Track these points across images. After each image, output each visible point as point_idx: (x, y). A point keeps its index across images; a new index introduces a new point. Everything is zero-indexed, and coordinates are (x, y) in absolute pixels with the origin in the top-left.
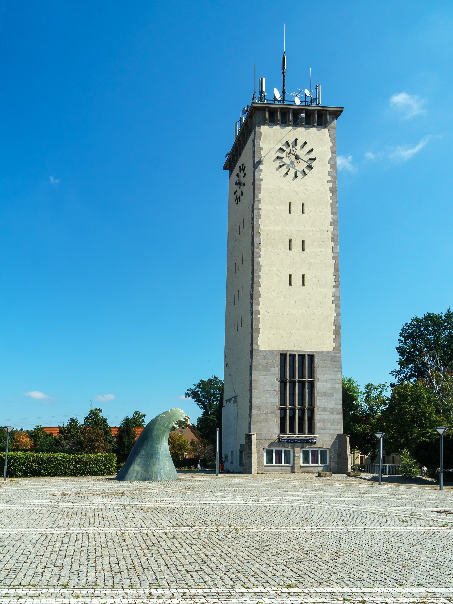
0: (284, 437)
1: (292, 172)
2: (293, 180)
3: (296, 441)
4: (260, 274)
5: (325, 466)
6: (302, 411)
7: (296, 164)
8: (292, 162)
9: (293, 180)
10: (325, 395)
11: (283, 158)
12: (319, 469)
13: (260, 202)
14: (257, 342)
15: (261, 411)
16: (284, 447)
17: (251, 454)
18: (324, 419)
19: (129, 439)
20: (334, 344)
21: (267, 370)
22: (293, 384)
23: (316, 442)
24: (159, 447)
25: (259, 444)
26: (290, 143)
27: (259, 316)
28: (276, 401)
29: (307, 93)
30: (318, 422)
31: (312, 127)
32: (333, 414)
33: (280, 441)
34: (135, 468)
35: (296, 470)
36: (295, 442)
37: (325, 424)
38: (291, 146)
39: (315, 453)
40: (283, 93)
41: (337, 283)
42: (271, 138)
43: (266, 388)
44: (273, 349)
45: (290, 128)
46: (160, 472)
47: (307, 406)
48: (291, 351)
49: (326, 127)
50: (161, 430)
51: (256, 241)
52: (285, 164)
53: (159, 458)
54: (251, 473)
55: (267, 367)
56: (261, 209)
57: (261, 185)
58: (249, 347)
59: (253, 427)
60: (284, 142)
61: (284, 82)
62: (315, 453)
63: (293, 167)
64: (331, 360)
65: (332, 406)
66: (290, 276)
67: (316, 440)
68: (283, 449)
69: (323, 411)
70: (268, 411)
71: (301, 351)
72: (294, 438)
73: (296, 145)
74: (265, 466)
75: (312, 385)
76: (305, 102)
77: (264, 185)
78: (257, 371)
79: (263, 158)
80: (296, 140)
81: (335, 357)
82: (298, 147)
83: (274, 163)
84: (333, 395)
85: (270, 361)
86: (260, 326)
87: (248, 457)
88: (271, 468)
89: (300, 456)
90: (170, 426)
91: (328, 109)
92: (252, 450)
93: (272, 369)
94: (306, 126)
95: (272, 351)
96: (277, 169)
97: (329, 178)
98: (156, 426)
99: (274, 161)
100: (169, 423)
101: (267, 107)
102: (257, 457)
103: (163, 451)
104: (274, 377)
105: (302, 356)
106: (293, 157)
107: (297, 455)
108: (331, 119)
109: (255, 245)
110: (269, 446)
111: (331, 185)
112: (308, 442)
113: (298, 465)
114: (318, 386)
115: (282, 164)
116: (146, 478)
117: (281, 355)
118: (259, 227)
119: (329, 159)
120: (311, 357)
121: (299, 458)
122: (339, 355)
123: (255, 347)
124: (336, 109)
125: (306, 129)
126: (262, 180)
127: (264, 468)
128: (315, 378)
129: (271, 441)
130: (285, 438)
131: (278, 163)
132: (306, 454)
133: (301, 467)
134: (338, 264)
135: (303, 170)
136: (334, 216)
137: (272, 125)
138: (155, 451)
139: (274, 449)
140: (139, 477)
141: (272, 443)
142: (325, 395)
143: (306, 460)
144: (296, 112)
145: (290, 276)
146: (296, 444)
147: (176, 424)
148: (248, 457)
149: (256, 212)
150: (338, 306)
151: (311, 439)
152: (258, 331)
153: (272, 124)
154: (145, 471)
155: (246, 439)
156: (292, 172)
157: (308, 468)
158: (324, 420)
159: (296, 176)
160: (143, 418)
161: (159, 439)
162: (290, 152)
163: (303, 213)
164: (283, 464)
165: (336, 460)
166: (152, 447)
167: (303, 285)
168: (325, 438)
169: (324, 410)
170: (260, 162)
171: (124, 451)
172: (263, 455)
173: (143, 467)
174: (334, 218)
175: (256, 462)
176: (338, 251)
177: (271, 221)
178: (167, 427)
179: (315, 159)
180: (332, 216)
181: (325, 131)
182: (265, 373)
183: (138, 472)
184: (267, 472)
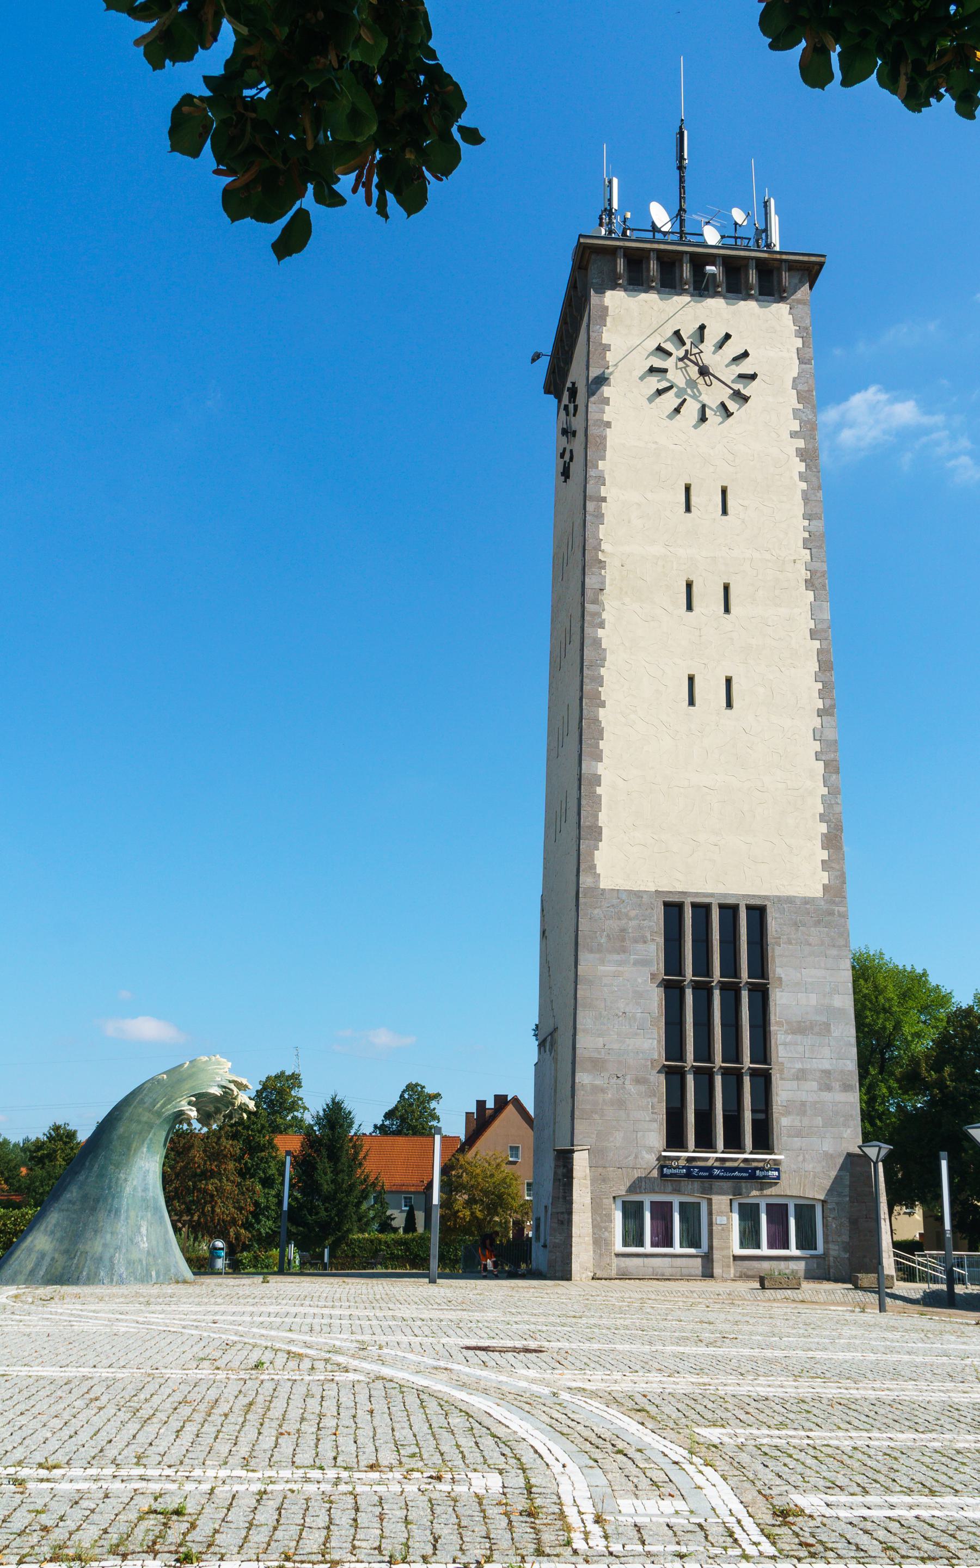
0: (678, 1158)
1: (691, 409)
2: (695, 427)
3: (716, 1172)
4: (603, 671)
5: (812, 1257)
6: (733, 1078)
7: (702, 387)
8: (692, 383)
9: (695, 427)
10: (801, 1028)
11: (665, 371)
12: (793, 1265)
13: (601, 480)
14: (593, 867)
15: (606, 1075)
16: (677, 1191)
17: (570, 1213)
18: (803, 1104)
19: (336, 1172)
20: (824, 877)
21: (623, 950)
22: (702, 990)
23: (778, 1178)
24: (122, 1176)
25: (598, 1180)
26: (684, 335)
27: (599, 790)
28: (652, 1044)
29: (738, 215)
30: (783, 1115)
31: (745, 300)
32: (829, 1088)
33: (667, 1174)
34: (37, 1242)
35: (717, 1271)
36: (711, 1176)
37: (806, 1121)
38: (688, 342)
39: (778, 1213)
40: (679, 215)
41: (828, 702)
42: (630, 323)
43: (621, 1005)
44: (642, 888)
45: (687, 298)
46: (111, 1258)
47: (747, 1063)
48: (697, 894)
49: (782, 299)
50: (139, 1122)
51: (590, 581)
52: (671, 388)
53: (117, 1212)
54: (569, 1278)
55: (623, 940)
56: (604, 499)
57: (605, 438)
58: (574, 878)
59: (579, 1126)
60: (670, 333)
61: (682, 188)
62: (778, 1213)
63: (694, 397)
64: (818, 923)
65: (826, 1065)
66: (691, 679)
67: (777, 1170)
68: (676, 1200)
69: (798, 1079)
70: (628, 1077)
71: (725, 895)
72: (709, 1164)
73: (702, 341)
74: (617, 1255)
75: (761, 996)
76: (736, 238)
77: (613, 438)
78: (591, 951)
79: (611, 370)
80: (702, 327)
81: (830, 910)
82: (708, 346)
83: (642, 384)
84: (829, 1031)
85: (632, 924)
86: (603, 819)
87: (562, 1223)
88: (639, 1261)
89: (727, 1224)
90: (170, 1109)
91: (784, 257)
92: (571, 1202)
93: (640, 946)
94: (729, 295)
95: (638, 894)
96: (651, 400)
97: (796, 426)
98: (130, 1110)
99: (642, 378)
100: (169, 1101)
101: (620, 247)
102: (592, 1224)
103: (135, 1189)
104: (646, 972)
105: (729, 911)
106: (693, 370)
107: (719, 1220)
108: (796, 281)
109: (589, 593)
110: (632, 1189)
111: (801, 443)
112: (753, 1176)
113: (725, 1253)
114: (781, 1002)
115: (665, 384)
116: (62, 1275)
117: (666, 904)
118: (600, 545)
119: (795, 380)
120: (758, 913)
121: (727, 1228)
122: (842, 909)
123: (586, 881)
124: (806, 259)
125: (727, 304)
126: (608, 425)
127: (615, 1260)
128: (771, 975)
129: (637, 1174)
130: (682, 1163)
131: (655, 383)
132: (749, 1214)
133: (736, 1258)
134: (828, 651)
135: (723, 405)
136: (814, 523)
137: (635, 291)
138: (110, 1188)
139: (647, 1199)
140: (42, 1273)
141: (640, 1179)
142: (801, 1028)
143: (750, 1237)
144: (699, 261)
145: (691, 679)
146: (717, 1184)
147: (189, 1103)
148: (562, 1223)
149: (590, 506)
150: (831, 767)
151: (762, 1169)
152: (597, 833)
153: (636, 287)
154: (67, 1252)
155: (556, 1167)
156: (691, 409)
157: (756, 1264)
158: (801, 1108)
159: (703, 419)
160: (433, 1104)
161: (129, 1149)
162: (686, 357)
163: (725, 512)
164: (677, 1249)
165: (846, 1238)
166: (101, 1175)
167: (729, 704)
168: (809, 1166)
169: (801, 1076)
170: (602, 380)
171: (317, 1213)
172: (609, 1219)
173: (61, 1240)
174: (812, 528)
175: (589, 1239)
176: (827, 615)
177: (634, 527)
178: (159, 1114)
179: (753, 377)
180: (806, 523)
181: (781, 310)
182: (616, 957)
183: (43, 1255)
184: (624, 1276)
